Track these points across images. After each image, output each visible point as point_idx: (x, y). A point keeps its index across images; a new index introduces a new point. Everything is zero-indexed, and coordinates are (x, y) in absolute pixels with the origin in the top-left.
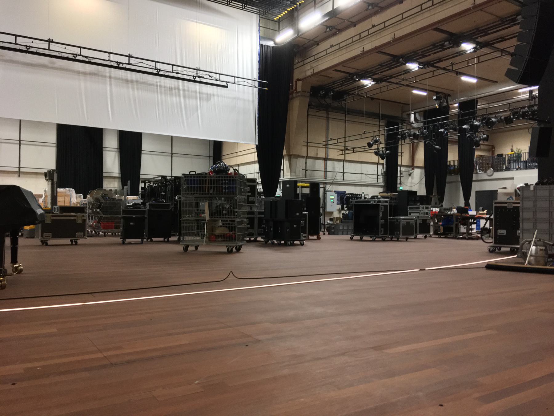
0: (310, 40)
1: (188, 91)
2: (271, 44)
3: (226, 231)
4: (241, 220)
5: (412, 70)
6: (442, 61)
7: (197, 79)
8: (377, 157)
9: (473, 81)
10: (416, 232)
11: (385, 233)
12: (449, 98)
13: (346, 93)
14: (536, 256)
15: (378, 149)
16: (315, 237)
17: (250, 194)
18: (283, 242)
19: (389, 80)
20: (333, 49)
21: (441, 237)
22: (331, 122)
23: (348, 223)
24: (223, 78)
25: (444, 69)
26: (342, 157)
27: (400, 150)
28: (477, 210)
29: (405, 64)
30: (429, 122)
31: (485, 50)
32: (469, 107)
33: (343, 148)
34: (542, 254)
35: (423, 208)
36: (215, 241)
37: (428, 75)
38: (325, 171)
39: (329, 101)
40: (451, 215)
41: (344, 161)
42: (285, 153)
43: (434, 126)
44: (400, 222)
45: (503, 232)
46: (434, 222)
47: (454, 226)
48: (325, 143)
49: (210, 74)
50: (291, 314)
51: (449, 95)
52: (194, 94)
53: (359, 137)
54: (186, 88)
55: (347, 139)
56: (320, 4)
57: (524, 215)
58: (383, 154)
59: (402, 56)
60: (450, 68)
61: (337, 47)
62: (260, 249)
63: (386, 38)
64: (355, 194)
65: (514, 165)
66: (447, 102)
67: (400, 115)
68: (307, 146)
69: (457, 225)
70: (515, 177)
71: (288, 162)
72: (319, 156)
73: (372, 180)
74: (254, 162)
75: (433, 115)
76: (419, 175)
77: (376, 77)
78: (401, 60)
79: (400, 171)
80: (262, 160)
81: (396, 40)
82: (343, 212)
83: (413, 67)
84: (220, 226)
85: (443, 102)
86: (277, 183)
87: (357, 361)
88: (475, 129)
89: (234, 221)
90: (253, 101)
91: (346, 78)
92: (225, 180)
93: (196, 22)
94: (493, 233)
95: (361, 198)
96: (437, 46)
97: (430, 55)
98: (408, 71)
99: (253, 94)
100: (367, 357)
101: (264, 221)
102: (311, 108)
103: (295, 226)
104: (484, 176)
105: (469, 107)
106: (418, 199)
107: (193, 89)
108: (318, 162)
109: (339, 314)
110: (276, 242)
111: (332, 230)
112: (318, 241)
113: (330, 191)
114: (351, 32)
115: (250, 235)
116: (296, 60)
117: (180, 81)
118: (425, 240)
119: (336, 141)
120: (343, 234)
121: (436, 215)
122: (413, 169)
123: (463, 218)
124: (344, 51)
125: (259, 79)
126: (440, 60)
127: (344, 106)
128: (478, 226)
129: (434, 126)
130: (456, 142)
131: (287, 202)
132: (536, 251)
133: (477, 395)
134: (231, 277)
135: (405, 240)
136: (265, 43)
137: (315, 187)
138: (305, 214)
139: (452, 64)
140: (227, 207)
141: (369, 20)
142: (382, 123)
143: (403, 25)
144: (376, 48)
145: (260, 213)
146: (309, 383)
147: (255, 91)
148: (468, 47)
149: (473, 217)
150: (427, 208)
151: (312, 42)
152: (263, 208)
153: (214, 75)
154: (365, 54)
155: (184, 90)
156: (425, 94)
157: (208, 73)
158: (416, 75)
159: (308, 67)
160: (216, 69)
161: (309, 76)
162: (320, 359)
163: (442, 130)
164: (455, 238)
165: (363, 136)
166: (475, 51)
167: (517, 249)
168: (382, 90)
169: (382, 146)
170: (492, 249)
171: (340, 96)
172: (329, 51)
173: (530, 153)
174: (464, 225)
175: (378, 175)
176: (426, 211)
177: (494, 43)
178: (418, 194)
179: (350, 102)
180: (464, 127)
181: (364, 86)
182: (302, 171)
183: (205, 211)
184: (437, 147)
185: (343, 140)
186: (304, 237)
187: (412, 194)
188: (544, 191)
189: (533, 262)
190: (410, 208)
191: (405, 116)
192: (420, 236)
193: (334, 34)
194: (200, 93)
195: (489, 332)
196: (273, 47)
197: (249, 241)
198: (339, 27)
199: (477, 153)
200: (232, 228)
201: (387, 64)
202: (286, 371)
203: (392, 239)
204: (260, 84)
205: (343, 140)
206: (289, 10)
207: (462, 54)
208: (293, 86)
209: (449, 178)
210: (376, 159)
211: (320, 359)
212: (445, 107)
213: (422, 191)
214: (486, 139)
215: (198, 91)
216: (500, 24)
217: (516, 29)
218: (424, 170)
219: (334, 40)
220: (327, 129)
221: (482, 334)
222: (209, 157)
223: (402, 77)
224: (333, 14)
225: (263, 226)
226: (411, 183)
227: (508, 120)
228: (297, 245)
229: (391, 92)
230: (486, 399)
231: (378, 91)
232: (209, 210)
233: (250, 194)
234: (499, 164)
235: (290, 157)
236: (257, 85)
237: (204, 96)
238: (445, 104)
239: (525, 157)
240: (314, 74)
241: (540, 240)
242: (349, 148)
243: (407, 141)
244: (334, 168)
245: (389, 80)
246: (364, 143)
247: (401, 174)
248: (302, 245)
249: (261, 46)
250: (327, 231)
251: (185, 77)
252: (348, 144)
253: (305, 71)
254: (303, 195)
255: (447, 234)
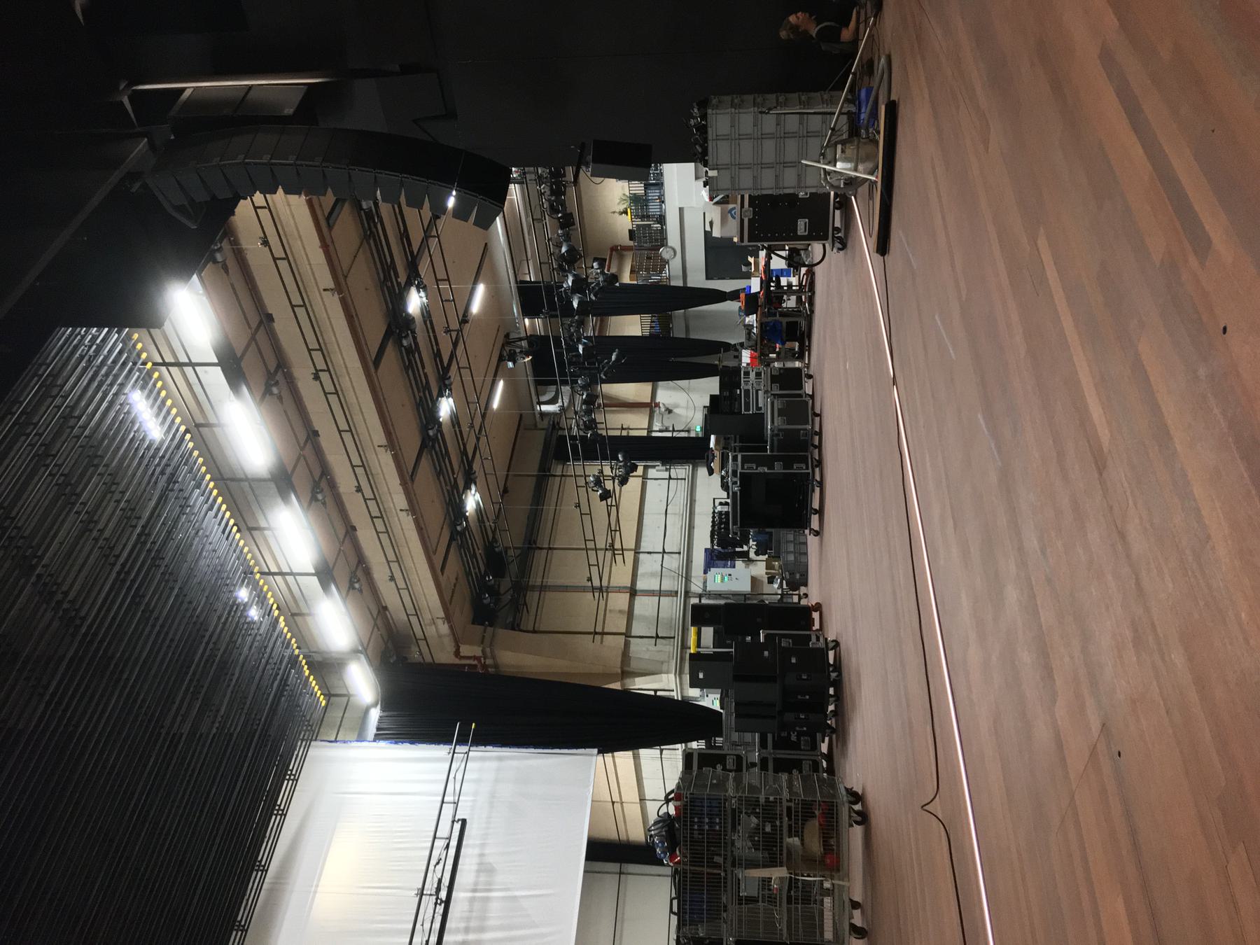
0: (376, 624)
1: (468, 919)
2: (375, 715)
3: (813, 830)
4: (787, 787)
5: (452, 411)
6: (439, 350)
7: (443, 895)
8: (631, 479)
9: (481, 289)
10: (800, 396)
11: (804, 460)
12: (513, 336)
13: (490, 547)
14: (857, 161)
15: (613, 479)
16: (816, 615)
17: (719, 767)
18: (831, 691)
19: (470, 456)
20: (398, 575)
21: (809, 346)
22: (551, 581)
23: (779, 542)
24: (444, 831)
25: (455, 344)
26: (629, 556)
27: (617, 433)
28: (748, 276)
29: (440, 424)
30: (563, 374)
31: (424, 268)
32: (532, 298)
33: (609, 554)
34: (851, 150)
35: (747, 383)
36: (838, 854)
37: (467, 378)
38: (660, 593)
39: (506, 584)
40: (762, 325)
41: (637, 552)
42: (616, 686)
43: (570, 363)
44: (780, 430)
45: (802, 226)
46: (773, 360)
47: (785, 320)
48: (597, 595)
49: (433, 862)
50: (1026, 657)
51: (507, 336)
52: (477, 905)
53: (586, 519)
54: (462, 925)
55: (590, 545)
56: (302, 604)
57: (768, 185)
58: (625, 466)
59: (424, 429)
60: (454, 334)
61: (395, 566)
62: (851, 746)
63: (384, 464)
64: (713, 526)
65: (654, 209)
66: (521, 339)
67: (543, 432)
68: (603, 634)
69: (783, 315)
70: (678, 205)
71: (637, 679)
72: (626, 608)
73: (680, 490)
74: (636, 758)
75: (547, 364)
76: (669, 393)
77: (461, 484)
78: (431, 433)
79: (660, 431)
80: (633, 741)
81: (392, 443)
82: (752, 555)
83: (446, 407)
84: (802, 840)
85: (521, 347)
86: (686, 706)
87: (1135, 504)
88: (581, 285)
89: (789, 809)
90: (500, 759)
91: (460, 547)
92: (692, 823)
93: (315, 892)
94: (799, 244)
95: (727, 513)
96: (410, 361)
97: (425, 375)
98: (455, 419)
99: (482, 759)
100: (1126, 484)
101: (784, 734)
102: (518, 625)
103: (794, 661)
104: (675, 265)
105: (532, 298)
106: (726, 394)
107: (466, 906)
108: (638, 610)
109: (1021, 549)
110: (831, 708)
111: (797, 579)
112: (824, 609)
113: (705, 582)
114: (367, 537)
115: (816, 766)
116: (415, 656)
117: (445, 938)
118: (817, 377)
119: (594, 570)
120: (806, 554)
121: (762, 358)
122: (657, 405)
123: (767, 301)
124: (405, 551)
125: (450, 742)
126: (437, 355)
127: (518, 552)
128: (781, 272)
129: (570, 363)
130: (602, 321)
131: (739, 678)
132: (846, 160)
133: (1193, 261)
134: (936, 807)
135: (817, 419)
136: (372, 729)
137: (701, 615)
138: (766, 637)
139: (448, 331)
140: (754, 820)
141: (345, 498)
142: (558, 470)
143: (361, 429)
144: (404, 483)
145: (763, 744)
146: (1202, 603)
147: (477, 753)
148: (415, 302)
149: (765, 284)
150: (747, 374)
151: (379, 622)
152: (748, 737)
153: (436, 854)
154: (413, 508)
155: (467, 930)
156: (501, 385)
157: (431, 867)
158: (463, 401)
159: (431, 631)
160: (423, 848)
161: (451, 628)
162: (1138, 583)
163: (581, 348)
164: (810, 319)
165: (585, 509)
166: (425, 288)
167: (836, 195)
168: (489, 470)
169: (607, 471)
170: (838, 245)
171: (495, 561)
172: (401, 584)
173: (630, 178)
174: (781, 300)
175: (670, 478)
176: (752, 375)
177: (412, 252)
178: (717, 392)
179: (510, 540)
180: (575, 304)
181: (478, 510)
182: (659, 647)
183: (764, 880)
184: (614, 358)
185: (592, 554)
186: (818, 639)
187: (715, 407)
188: (720, 151)
189: (870, 165)
190: (747, 409)
191: (545, 424)
192: (808, 389)
193: (368, 573)
194: (475, 891)
195: (1042, 242)
196: (383, 710)
197: (831, 770)
198: (354, 561)
199: (626, 279)
200: (806, 811)
201: (436, 459)
202: (1178, 658)
203: (815, 447)
204: (462, 741)
205: (592, 554)
206: (307, 673)
207: (429, 313)
208: (469, 665)
209: (678, 332)
210: (634, 483)
211: (1138, 583)
212: (530, 344)
213: (711, 385)
214: (602, 262)
215: (469, 895)
216: (375, 240)
217: (385, 209)
218: (660, 383)
219: (380, 573)
220: (565, 589)
221: (1047, 257)
222: (621, 873)
223: (465, 429)
224: (325, 574)
225: (794, 738)
226: (687, 408)
227: (567, 222)
228: (838, 658)
229: (493, 452)
230: (1202, 245)
231: (491, 479)
232: (765, 866)
233: (719, 767)
234: (649, 237)
235: (626, 674)
236: (464, 749)
237: (482, 879)
238: (524, 343)
239: (638, 188)
240: (448, 618)
241: (823, 155)
242: (610, 541)
243: (599, 417)
244: (652, 575)
245: (470, 456)
246: (600, 507)
247: (667, 430)
248: (837, 644)
249: (378, 737)
250: (798, 589)
251: (437, 925)
252: (601, 543)
253: (440, 636)
254: (718, 642)
255: (802, 334)
